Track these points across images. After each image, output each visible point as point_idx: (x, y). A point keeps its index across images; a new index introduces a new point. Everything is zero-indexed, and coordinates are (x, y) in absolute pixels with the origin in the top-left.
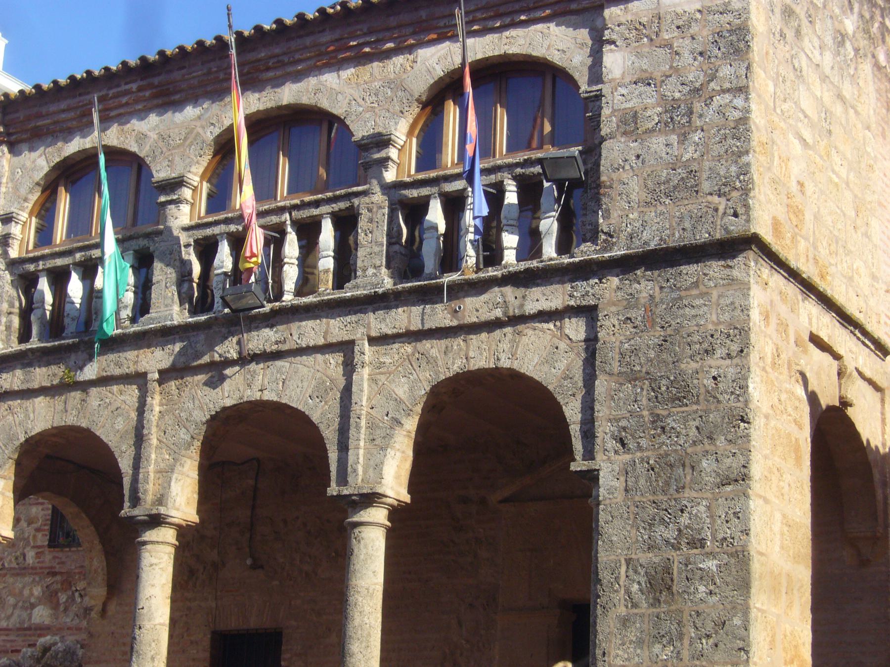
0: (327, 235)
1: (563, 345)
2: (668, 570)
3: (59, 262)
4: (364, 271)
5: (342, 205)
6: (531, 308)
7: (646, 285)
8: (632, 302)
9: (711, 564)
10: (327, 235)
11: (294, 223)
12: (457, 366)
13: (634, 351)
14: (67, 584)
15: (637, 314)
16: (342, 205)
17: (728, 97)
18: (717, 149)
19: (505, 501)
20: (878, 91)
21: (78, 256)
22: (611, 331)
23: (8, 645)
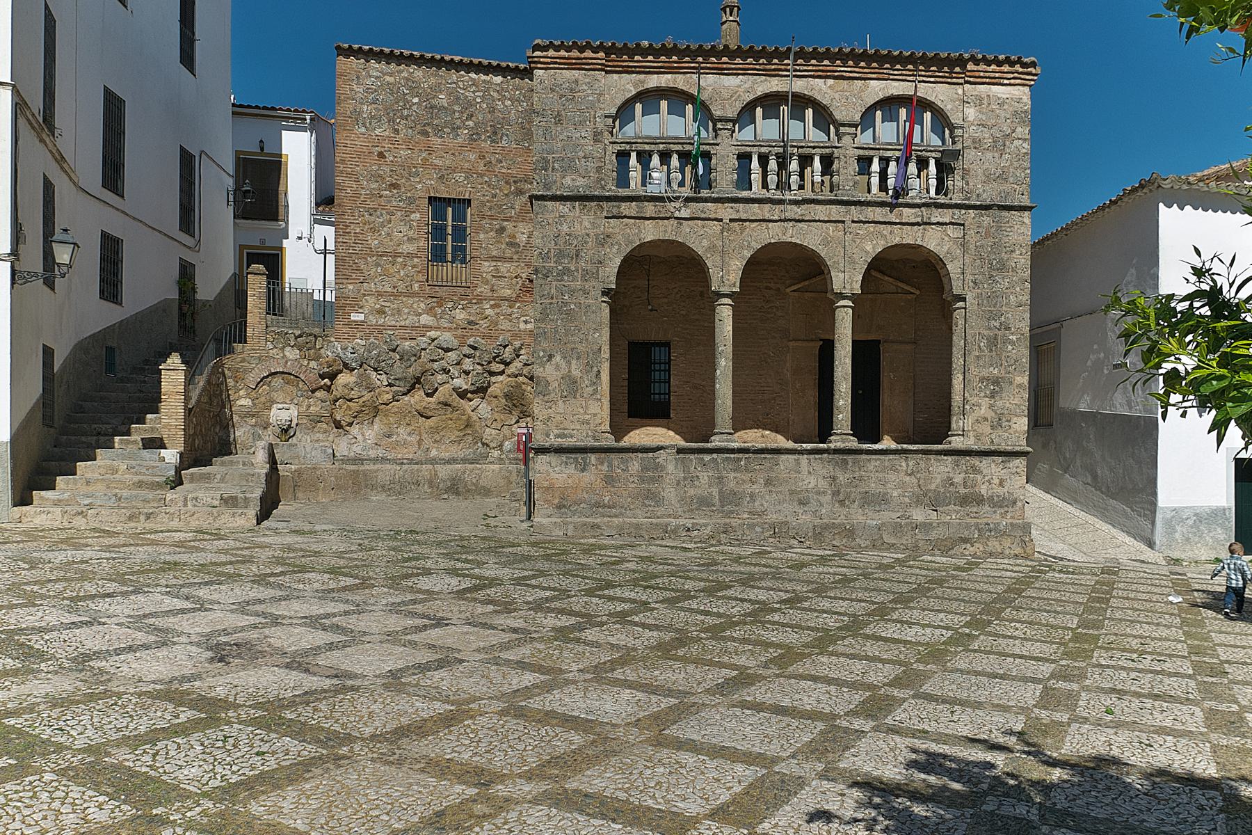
0: (773, 165)
2: (995, 339)
3: (647, 147)
5: (828, 151)
6: (934, 220)
7: (986, 219)
9: (1014, 338)
10: (773, 165)
11: (800, 156)
12: (897, 241)
13: (982, 246)
15: (983, 231)
16: (828, 151)
18: (1016, 165)
20: (244, 667)
22: (972, 237)
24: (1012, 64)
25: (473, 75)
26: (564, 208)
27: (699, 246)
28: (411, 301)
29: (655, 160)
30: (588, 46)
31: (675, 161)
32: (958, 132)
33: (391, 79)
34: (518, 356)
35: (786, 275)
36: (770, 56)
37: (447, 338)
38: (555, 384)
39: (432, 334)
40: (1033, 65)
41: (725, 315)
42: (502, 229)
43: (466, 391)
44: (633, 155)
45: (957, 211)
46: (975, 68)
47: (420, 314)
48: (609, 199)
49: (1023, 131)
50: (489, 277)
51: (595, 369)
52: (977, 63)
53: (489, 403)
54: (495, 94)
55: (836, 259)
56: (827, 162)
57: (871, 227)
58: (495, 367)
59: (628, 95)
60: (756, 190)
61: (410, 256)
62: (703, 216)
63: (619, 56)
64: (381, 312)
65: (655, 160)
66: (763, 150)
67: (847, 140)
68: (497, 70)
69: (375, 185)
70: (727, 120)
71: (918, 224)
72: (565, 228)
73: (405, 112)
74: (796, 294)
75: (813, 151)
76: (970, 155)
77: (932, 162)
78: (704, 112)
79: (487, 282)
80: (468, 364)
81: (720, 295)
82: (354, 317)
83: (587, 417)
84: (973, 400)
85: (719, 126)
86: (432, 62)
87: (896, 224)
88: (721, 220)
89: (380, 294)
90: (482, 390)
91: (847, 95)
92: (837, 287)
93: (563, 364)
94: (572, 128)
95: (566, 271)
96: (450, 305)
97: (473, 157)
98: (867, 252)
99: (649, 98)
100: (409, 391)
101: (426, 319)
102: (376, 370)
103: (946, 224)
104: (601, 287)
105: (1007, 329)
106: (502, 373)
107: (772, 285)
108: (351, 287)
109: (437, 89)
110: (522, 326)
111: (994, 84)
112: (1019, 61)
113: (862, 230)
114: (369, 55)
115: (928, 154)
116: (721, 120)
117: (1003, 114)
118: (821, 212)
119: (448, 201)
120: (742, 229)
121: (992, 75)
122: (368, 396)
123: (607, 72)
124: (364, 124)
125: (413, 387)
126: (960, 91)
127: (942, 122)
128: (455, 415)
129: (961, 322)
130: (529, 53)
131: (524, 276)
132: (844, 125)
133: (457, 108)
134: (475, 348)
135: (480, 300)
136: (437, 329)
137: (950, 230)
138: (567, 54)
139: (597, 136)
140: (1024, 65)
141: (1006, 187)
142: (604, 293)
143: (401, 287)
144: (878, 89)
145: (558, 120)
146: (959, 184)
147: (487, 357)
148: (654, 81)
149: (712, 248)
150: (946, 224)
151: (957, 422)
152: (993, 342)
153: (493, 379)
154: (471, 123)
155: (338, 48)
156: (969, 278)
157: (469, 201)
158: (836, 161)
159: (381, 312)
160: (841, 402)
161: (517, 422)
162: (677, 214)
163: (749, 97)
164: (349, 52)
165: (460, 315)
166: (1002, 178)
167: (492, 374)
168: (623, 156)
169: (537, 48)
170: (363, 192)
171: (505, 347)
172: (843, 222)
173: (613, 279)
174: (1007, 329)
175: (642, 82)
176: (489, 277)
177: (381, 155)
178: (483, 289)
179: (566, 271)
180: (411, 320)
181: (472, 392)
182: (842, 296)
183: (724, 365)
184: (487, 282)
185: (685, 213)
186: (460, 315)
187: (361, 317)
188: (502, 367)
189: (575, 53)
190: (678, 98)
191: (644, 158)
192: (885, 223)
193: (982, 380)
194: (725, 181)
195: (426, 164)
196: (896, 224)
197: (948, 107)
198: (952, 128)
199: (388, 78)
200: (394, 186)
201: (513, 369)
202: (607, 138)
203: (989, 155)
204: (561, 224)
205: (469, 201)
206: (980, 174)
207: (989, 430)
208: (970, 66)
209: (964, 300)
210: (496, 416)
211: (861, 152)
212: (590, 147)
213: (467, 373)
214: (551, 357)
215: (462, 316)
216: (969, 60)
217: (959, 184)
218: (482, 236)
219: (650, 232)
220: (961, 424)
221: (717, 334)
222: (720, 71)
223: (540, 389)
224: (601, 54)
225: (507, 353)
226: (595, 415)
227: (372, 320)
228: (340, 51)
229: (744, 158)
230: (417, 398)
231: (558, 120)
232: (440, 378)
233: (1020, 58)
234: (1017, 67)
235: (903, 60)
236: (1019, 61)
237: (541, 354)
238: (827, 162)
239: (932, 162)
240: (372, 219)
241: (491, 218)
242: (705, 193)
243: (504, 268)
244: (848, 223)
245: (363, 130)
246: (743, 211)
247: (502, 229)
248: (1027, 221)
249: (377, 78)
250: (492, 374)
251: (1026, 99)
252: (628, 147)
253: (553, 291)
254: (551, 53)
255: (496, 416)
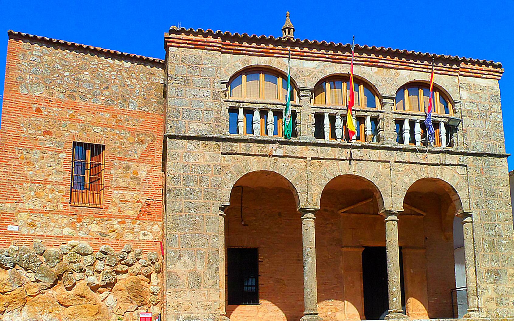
1: (456, 175)
2: (493, 243)
3: (251, 106)
4: (387, 138)
7: (480, 162)
8: (476, 166)
10: (339, 122)
12: (425, 176)
14: (79, 221)
16: (375, 114)
17: (496, 114)
19: (343, 212)
21: (261, 106)
23: (52, 243)
24: (487, 65)
25: (110, 60)
26: (191, 145)
27: (291, 176)
28: (56, 217)
29: (257, 114)
30: (210, 33)
31: (271, 116)
32: (457, 106)
33: (49, 58)
34: (138, 260)
35: (351, 199)
36: (336, 49)
37: (84, 245)
38: (184, 278)
39: (73, 242)
40: (500, 66)
41: (309, 225)
42: (128, 167)
43: (98, 286)
44: (241, 111)
45: (461, 157)
46: (466, 66)
47: (63, 227)
48: (225, 140)
49: (497, 107)
50: (117, 201)
51: (215, 266)
52: (466, 63)
53: (115, 295)
54: (125, 74)
55: (385, 187)
56: (375, 120)
57: (407, 166)
58: (120, 268)
59: (238, 69)
60: (328, 139)
61: (58, 183)
62: (293, 155)
63: (232, 41)
64: (32, 225)
65: (257, 114)
66: (333, 112)
67: (387, 108)
68: (127, 58)
69: (33, 132)
70: (307, 90)
71: (437, 165)
72: (191, 160)
73: (58, 82)
74: (345, 215)
75: (366, 114)
76: (466, 121)
77: (442, 125)
78: (291, 83)
79: (116, 205)
80: (99, 265)
81: (305, 211)
82: (10, 228)
83: (209, 303)
84: (483, 286)
85: (302, 93)
86: (80, 49)
87: (423, 164)
88: (306, 158)
89: (31, 211)
90: (110, 285)
91: (388, 78)
92: (387, 207)
93: (190, 262)
94: (196, 89)
95: (192, 192)
96: (87, 221)
97: (107, 115)
98: (406, 183)
99: (251, 71)
100: (52, 286)
101: (67, 231)
102: (26, 269)
103: (456, 165)
104: (219, 204)
105: (500, 236)
106: (127, 271)
107: (328, 208)
108: (9, 205)
109: (80, 69)
110: (142, 237)
111: (476, 77)
112: (491, 64)
113: (402, 168)
114: (33, 40)
115: (439, 119)
116: (303, 90)
117: (484, 96)
118: (374, 154)
119: (86, 146)
120: (320, 165)
121: (476, 71)
122: (18, 290)
123: (222, 52)
124: (26, 88)
125: (55, 283)
126: (457, 81)
127: (445, 98)
128: (89, 304)
129: (470, 231)
130: (166, 34)
131: (143, 201)
132: (385, 98)
133: (97, 81)
134: (105, 253)
135: (111, 217)
136: (76, 239)
137: (458, 169)
138: (194, 38)
139: (215, 97)
140: (495, 66)
141: (490, 143)
142: (221, 209)
143: (49, 206)
144: (406, 76)
145: (187, 82)
146: (461, 139)
147: (114, 260)
148: (256, 61)
149: (300, 178)
150: (456, 165)
151: (473, 302)
152: (492, 245)
153: (119, 277)
154: (107, 93)
155: (10, 34)
156: (473, 201)
157: (104, 146)
158: (381, 121)
159: (32, 225)
160: (395, 289)
161: (137, 309)
162: (274, 153)
163: (321, 76)
164: (18, 37)
165: (95, 228)
166: (487, 136)
167: (117, 273)
168: (233, 111)
169: (172, 32)
170: (23, 135)
171: (128, 253)
172: (389, 162)
173: (228, 198)
174: (500, 236)
175: (248, 61)
176: (117, 201)
177: (38, 110)
178: (112, 210)
179: (192, 192)
180: (56, 231)
181: (103, 287)
182: (390, 213)
183: (310, 263)
184: (116, 205)
185: (280, 152)
186: (95, 228)
187: (16, 229)
188: (126, 268)
189: (200, 37)
190: (273, 73)
191: (249, 112)
192: (416, 163)
193: (488, 271)
194: (307, 131)
195: (72, 119)
196: (423, 164)
197: (450, 90)
198: (453, 103)
199: (46, 57)
200: (46, 133)
201: (136, 267)
202: (222, 98)
203: (478, 122)
204: (188, 157)
205: (104, 146)
206: (471, 135)
207: (495, 307)
208: (462, 65)
209: (471, 216)
210: (120, 305)
211: (397, 116)
212: (210, 103)
213: (99, 272)
214: (180, 257)
215: (96, 230)
216: (462, 61)
217: (461, 139)
218: (113, 171)
219: (255, 165)
220: (476, 303)
221: (304, 240)
222: (301, 57)
223: (171, 282)
224: (219, 40)
225: (130, 258)
226: (215, 302)
227: (25, 231)
228: (11, 35)
229: (319, 117)
230: (59, 291)
231: (187, 82)
232: (78, 275)
233: (492, 62)
234: (491, 68)
235: (422, 58)
236: (491, 64)
237: (173, 254)
238: (375, 120)
239: (442, 125)
240: (28, 156)
241: (120, 158)
242: (293, 139)
243: (129, 195)
244: (392, 162)
245: (25, 92)
246: (320, 152)
247: (128, 167)
248: (506, 164)
249: (39, 56)
250: (117, 273)
251: (497, 88)
252: (237, 105)
253: (182, 206)
254: (183, 36)
255: (120, 305)
